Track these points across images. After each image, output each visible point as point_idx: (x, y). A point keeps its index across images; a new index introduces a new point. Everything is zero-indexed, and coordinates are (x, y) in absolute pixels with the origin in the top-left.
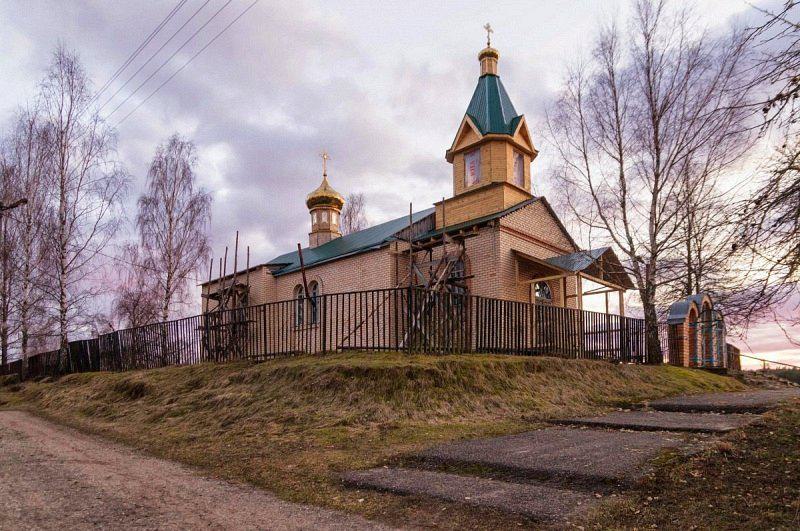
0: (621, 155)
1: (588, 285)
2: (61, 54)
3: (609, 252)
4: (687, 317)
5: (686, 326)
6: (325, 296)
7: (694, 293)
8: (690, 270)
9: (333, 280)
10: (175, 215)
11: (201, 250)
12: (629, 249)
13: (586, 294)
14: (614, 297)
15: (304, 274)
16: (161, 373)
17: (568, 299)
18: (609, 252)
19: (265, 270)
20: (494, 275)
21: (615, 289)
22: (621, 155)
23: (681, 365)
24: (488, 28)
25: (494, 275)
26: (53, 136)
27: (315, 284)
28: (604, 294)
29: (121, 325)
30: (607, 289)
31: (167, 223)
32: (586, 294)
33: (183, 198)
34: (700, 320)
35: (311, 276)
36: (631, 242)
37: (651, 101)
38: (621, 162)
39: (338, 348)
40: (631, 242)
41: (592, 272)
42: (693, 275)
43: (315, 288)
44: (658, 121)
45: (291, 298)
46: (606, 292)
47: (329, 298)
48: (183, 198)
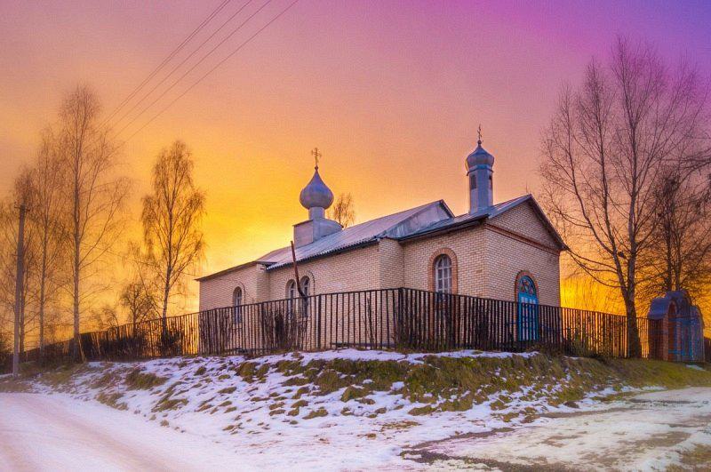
4: (666, 312)
5: (665, 321)
6: (315, 296)
7: (674, 288)
8: (670, 265)
9: (325, 280)
10: (175, 212)
12: (611, 249)
19: (259, 266)
20: (478, 272)
23: (639, 356)
25: (478, 272)
26: (452, 346)
27: (306, 280)
29: (123, 317)
31: (168, 220)
33: (185, 193)
34: (679, 315)
35: (302, 273)
36: (612, 239)
39: (331, 344)
40: (612, 239)
43: (307, 283)
45: (284, 297)
47: (323, 298)
48: (185, 193)
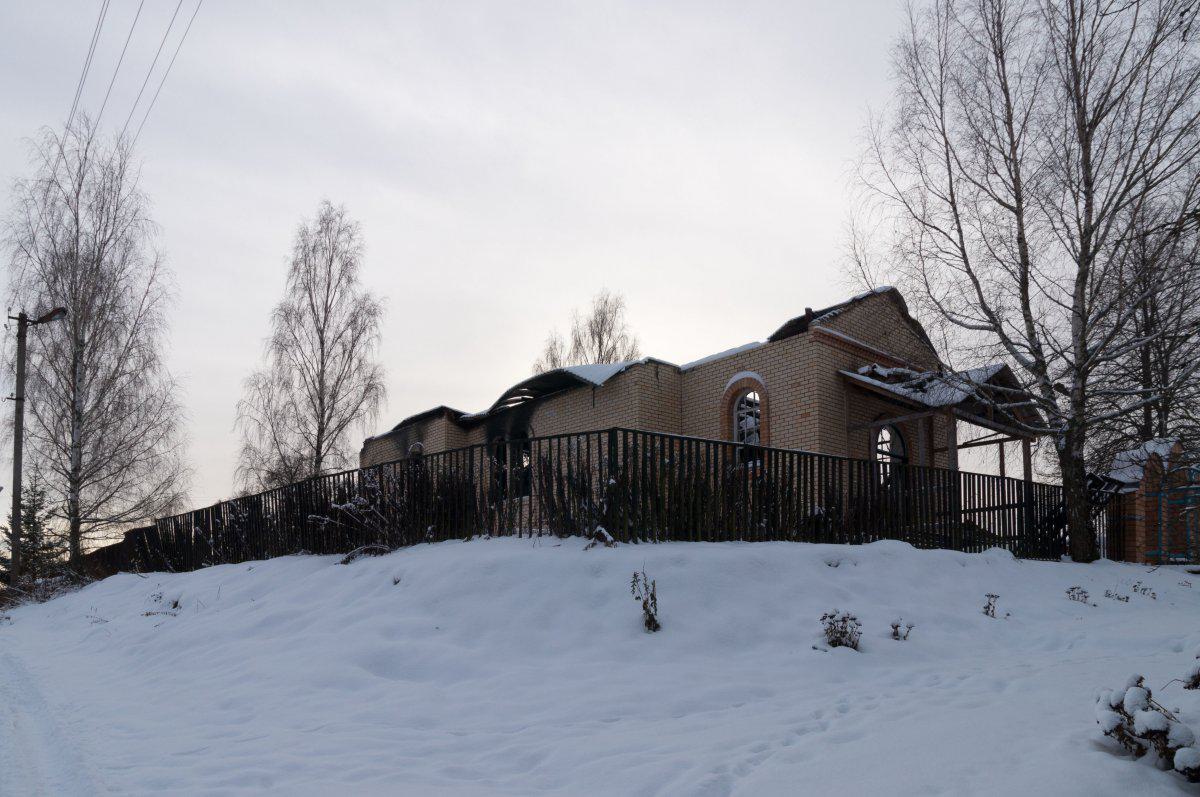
0: (1019, 199)
1: (965, 431)
2: (855, 646)
3: (1004, 376)
11: (369, 388)
13: (966, 445)
14: (1014, 451)
15: (550, 441)
16: (696, 499)
17: (937, 455)
18: (1004, 376)
21: (1014, 438)
22: (1019, 199)
24: (652, 624)
28: (995, 448)
30: (1001, 436)
32: (966, 445)
37: (1076, 95)
38: (1019, 212)
41: (972, 409)
42: (1154, 414)
44: (1090, 134)
46: (1001, 442)
